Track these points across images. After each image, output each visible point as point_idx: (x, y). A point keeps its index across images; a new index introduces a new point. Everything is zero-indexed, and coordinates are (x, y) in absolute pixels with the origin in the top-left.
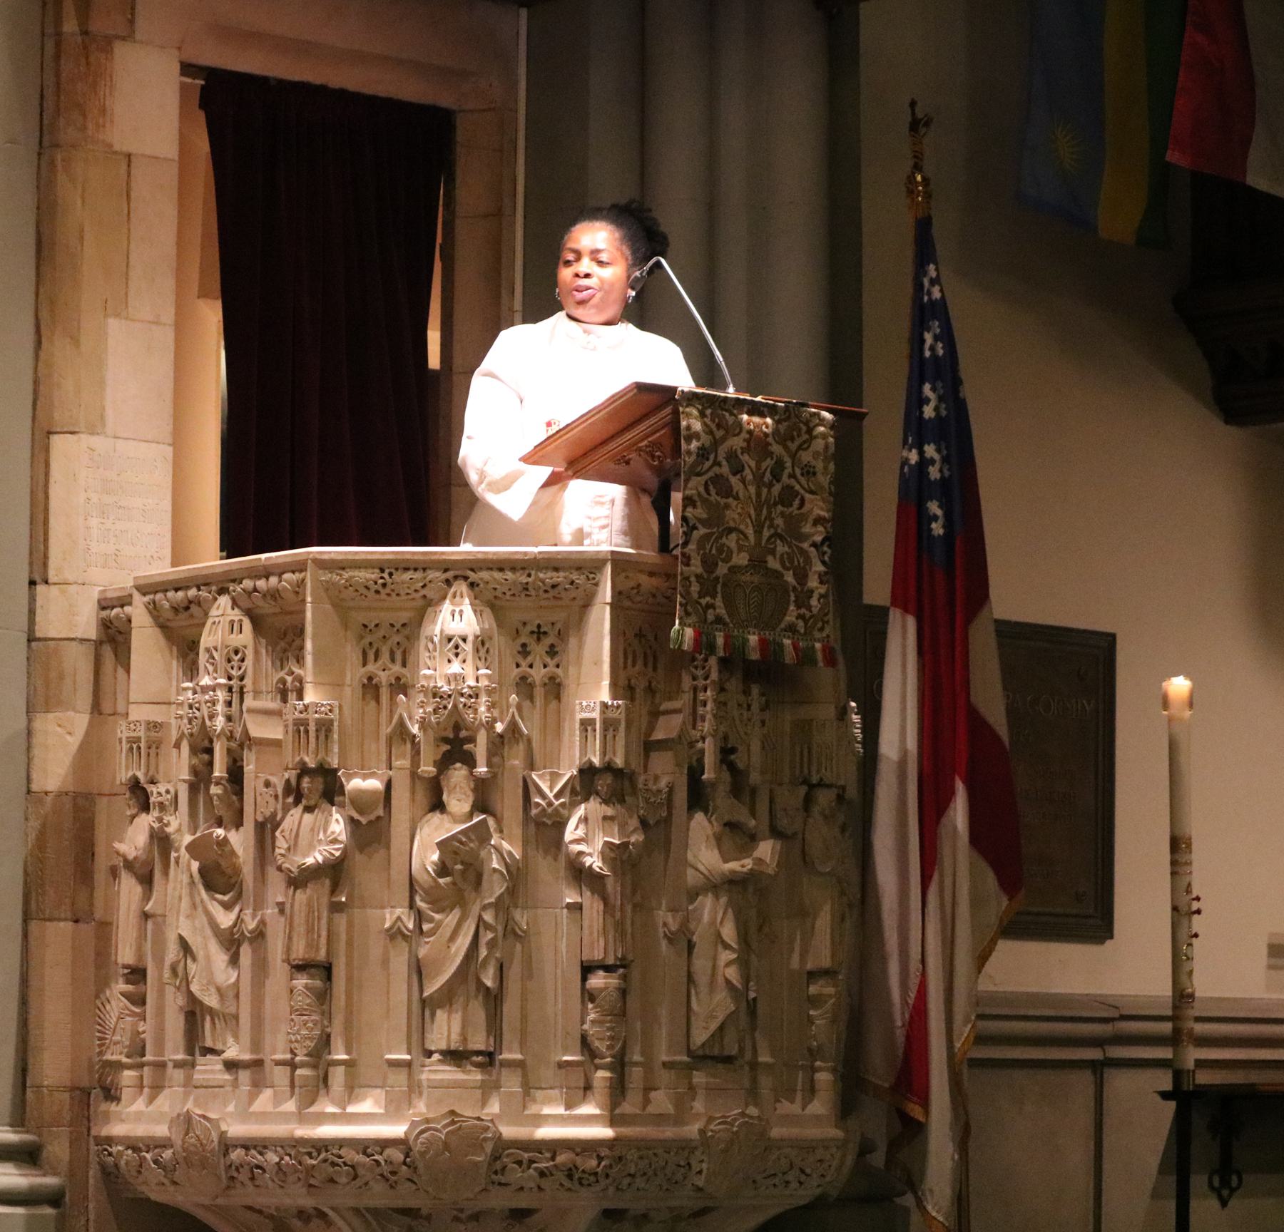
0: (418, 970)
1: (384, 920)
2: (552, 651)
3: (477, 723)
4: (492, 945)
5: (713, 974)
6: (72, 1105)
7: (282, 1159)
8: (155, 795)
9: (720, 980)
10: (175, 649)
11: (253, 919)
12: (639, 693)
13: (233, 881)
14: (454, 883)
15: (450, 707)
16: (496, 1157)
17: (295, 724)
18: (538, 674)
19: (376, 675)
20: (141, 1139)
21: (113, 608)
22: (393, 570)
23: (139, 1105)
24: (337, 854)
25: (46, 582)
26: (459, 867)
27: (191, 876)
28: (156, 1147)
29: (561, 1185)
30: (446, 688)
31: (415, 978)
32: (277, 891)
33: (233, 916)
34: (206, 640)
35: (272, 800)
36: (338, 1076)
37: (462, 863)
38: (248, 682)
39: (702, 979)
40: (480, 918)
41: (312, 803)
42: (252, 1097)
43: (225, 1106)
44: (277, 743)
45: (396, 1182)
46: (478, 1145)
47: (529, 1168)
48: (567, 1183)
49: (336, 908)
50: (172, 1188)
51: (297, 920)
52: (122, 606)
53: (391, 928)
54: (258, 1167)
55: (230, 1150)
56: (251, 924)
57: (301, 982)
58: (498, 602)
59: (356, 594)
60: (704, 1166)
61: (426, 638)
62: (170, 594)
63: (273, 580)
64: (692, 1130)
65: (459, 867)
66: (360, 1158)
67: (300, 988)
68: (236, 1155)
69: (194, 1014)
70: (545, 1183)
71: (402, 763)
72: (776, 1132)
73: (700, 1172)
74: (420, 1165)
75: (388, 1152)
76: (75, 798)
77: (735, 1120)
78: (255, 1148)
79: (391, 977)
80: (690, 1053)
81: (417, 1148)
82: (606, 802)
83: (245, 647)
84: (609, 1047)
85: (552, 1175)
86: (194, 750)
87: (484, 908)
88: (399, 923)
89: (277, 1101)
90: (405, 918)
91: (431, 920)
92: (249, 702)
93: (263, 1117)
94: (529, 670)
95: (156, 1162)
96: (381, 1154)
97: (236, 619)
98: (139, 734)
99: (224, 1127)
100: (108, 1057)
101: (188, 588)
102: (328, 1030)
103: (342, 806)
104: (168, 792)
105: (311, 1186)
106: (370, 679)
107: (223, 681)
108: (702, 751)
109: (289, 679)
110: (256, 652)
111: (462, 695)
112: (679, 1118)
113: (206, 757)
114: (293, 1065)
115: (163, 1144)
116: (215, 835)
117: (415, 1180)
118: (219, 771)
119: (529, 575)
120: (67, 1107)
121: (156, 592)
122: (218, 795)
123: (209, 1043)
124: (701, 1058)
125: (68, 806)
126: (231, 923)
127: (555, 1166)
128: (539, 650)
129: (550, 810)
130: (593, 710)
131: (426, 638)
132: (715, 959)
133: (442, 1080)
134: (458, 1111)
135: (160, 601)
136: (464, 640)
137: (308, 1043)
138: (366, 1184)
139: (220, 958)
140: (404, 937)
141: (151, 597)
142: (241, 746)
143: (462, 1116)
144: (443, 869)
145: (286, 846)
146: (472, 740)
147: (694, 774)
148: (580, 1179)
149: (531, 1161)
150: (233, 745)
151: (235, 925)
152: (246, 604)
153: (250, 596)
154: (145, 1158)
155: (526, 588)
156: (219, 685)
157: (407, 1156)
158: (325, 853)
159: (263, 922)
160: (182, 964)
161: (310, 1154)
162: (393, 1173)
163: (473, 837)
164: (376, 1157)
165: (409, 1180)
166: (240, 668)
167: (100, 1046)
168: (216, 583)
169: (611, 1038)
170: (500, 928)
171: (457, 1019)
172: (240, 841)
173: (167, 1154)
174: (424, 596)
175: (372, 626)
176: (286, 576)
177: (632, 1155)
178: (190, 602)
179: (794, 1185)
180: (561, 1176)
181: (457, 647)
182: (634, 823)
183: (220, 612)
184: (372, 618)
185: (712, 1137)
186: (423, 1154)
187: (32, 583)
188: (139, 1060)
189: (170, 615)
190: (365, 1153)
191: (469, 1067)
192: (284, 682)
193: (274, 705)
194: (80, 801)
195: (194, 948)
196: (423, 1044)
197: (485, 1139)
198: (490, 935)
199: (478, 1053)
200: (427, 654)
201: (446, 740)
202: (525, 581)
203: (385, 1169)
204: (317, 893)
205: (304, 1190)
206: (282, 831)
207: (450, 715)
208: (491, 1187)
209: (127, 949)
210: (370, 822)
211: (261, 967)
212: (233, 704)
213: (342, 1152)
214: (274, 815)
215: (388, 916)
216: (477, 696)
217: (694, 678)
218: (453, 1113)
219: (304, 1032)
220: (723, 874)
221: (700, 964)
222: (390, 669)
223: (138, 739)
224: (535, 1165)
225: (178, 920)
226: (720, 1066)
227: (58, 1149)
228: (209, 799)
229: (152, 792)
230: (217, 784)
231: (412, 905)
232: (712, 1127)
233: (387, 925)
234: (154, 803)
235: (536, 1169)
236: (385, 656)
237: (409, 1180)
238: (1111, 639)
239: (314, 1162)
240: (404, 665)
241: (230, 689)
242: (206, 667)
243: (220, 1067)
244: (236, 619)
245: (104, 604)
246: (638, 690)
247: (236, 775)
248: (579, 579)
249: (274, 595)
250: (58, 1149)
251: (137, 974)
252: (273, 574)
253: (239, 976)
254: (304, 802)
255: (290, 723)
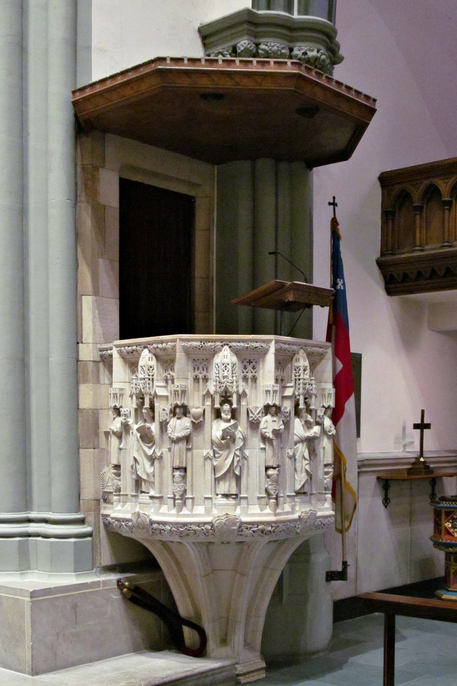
0: (215, 469)
1: (203, 454)
2: (254, 368)
3: (233, 391)
4: (238, 461)
5: (302, 468)
6: (94, 504)
7: (172, 528)
8: (123, 411)
9: (304, 470)
10: (127, 365)
11: (159, 452)
12: (279, 381)
13: (152, 440)
14: (227, 442)
15: (224, 386)
16: (240, 527)
17: (174, 392)
18: (250, 375)
19: (198, 375)
20: (121, 518)
21: (104, 351)
22: (205, 342)
23: (119, 507)
24: (189, 433)
25: (82, 343)
26: (228, 437)
27: (137, 438)
28: (126, 521)
29: (260, 535)
30: (223, 380)
31: (213, 472)
32: (167, 445)
33: (152, 451)
34: (141, 363)
35: (165, 415)
36: (189, 502)
37: (230, 436)
38: (155, 377)
39: (299, 469)
40: (235, 453)
41: (180, 416)
42: (160, 508)
43: (150, 510)
44: (167, 397)
45: (208, 535)
46: (234, 524)
47: (250, 530)
48: (261, 534)
49: (188, 450)
50: (131, 533)
51: (175, 454)
52: (107, 351)
53: (206, 455)
54: (163, 530)
55: (153, 524)
56: (159, 454)
57: (177, 473)
58: (237, 353)
59: (193, 350)
60: (300, 526)
61: (215, 364)
62: (127, 348)
63: (164, 345)
64: (296, 516)
65: (228, 437)
66: (197, 528)
67: (177, 475)
68: (155, 526)
69: (138, 482)
70: (254, 534)
71: (209, 403)
72: (319, 514)
73: (298, 528)
74: (216, 530)
75: (206, 526)
76: (93, 411)
77: (309, 512)
78: (162, 524)
79: (206, 472)
80: (295, 492)
81: (215, 525)
82: (273, 416)
83: (154, 366)
84: (275, 492)
85: (257, 532)
86: (137, 398)
87: (236, 450)
88: (208, 454)
89: (169, 509)
90: (210, 452)
91: (218, 453)
92: (156, 383)
93: (164, 514)
94: (247, 374)
95: (126, 525)
96: (204, 526)
97: (150, 356)
98: (117, 392)
99: (151, 517)
100: (106, 490)
101: (132, 346)
102: (186, 488)
103: (189, 417)
104: (127, 411)
105: (181, 536)
106: (196, 377)
107: (148, 377)
108: (299, 399)
109: (169, 376)
110: (157, 367)
111: (228, 382)
112: (293, 512)
113: (141, 400)
114: (174, 499)
115: (129, 520)
116: (146, 426)
117: (214, 534)
118: (147, 405)
119: (248, 344)
120: (93, 505)
121: (121, 347)
122: (145, 413)
123: (143, 490)
124: (298, 493)
125: (91, 413)
126: (151, 453)
127: (258, 529)
128: (250, 367)
129: (255, 419)
130: (270, 387)
131: (215, 364)
132: (302, 463)
133: (222, 503)
134: (229, 513)
135: (123, 350)
136: (228, 365)
137: (180, 492)
138: (199, 536)
139: (147, 464)
140: (210, 459)
141: (119, 348)
142: (154, 397)
143: (230, 515)
144: (223, 438)
145: (171, 430)
146: (231, 396)
147: (297, 405)
148: (266, 533)
149: (251, 528)
150: (152, 397)
151: (153, 453)
152: (153, 351)
153: (155, 350)
154: (122, 524)
155: (247, 348)
156: (146, 378)
157: (212, 527)
158: (185, 433)
159: (162, 453)
160: (134, 466)
161: (181, 527)
162: (208, 532)
163: (233, 428)
164: (202, 528)
165: (212, 534)
166: (152, 372)
167: (102, 486)
168: (143, 345)
169: (275, 490)
170: (241, 456)
171: (227, 484)
172: (154, 427)
173: (130, 524)
174: (214, 351)
175: (196, 360)
176: (169, 343)
177: (281, 525)
178: (133, 350)
179: (321, 528)
180: (260, 533)
181: (226, 367)
182: (281, 422)
183: (145, 354)
184: (196, 357)
185: (302, 518)
186: (217, 527)
187: (78, 343)
188: (118, 493)
189: (126, 354)
190: (199, 526)
191: (231, 499)
192: (167, 377)
193: (163, 384)
194: (95, 411)
195: (139, 461)
196: (216, 492)
197: (237, 522)
198: (238, 459)
199: (233, 495)
200: (216, 369)
201: (222, 396)
202: (247, 346)
203: (205, 531)
204: (183, 445)
205: (179, 538)
206: (170, 425)
207: (224, 389)
208: (238, 536)
209: (115, 459)
210: (198, 423)
211: (162, 468)
212: (150, 384)
213: (192, 526)
214: (166, 420)
215: (204, 452)
216: (233, 383)
217: (295, 376)
218: (227, 514)
219: (179, 489)
220: (305, 437)
221: (298, 465)
222: (202, 373)
223: (117, 394)
224: (252, 529)
225: (133, 452)
226: (303, 495)
227: (91, 518)
228: (142, 413)
229: (122, 411)
230: (145, 409)
231: (212, 448)
232: (303, 515)
233: (204, 455)
234: (123, 414)
235: (252, 530)
236: (201, 369)
237: (212, 534)
238: (361, 355)
239: (182, 530)
240: (207, 372)
241: (149, 379)
242: (141, 372)
243: (148, 498)
244: (150, 356)
245: (101, 350)
246: (279, 380)
247: (152, 408)
248: (264, 345)
249: (164, 349)
250: (91, 518)
251: (117, 467)
252: (164, 343)
253: (154, 468)
254: (177, 416)
255: (173, 391)
